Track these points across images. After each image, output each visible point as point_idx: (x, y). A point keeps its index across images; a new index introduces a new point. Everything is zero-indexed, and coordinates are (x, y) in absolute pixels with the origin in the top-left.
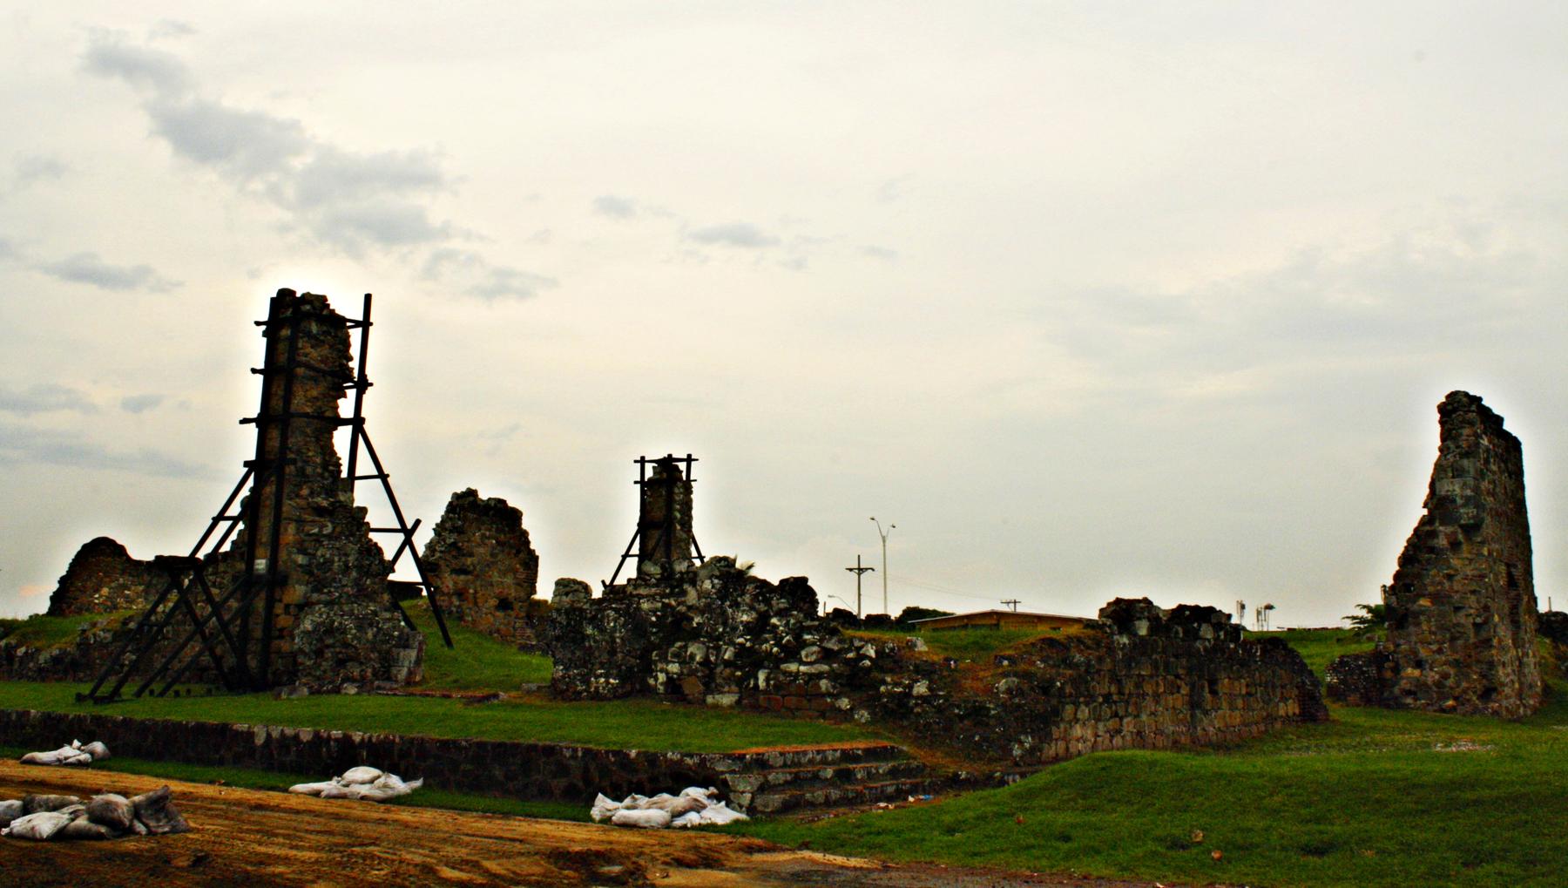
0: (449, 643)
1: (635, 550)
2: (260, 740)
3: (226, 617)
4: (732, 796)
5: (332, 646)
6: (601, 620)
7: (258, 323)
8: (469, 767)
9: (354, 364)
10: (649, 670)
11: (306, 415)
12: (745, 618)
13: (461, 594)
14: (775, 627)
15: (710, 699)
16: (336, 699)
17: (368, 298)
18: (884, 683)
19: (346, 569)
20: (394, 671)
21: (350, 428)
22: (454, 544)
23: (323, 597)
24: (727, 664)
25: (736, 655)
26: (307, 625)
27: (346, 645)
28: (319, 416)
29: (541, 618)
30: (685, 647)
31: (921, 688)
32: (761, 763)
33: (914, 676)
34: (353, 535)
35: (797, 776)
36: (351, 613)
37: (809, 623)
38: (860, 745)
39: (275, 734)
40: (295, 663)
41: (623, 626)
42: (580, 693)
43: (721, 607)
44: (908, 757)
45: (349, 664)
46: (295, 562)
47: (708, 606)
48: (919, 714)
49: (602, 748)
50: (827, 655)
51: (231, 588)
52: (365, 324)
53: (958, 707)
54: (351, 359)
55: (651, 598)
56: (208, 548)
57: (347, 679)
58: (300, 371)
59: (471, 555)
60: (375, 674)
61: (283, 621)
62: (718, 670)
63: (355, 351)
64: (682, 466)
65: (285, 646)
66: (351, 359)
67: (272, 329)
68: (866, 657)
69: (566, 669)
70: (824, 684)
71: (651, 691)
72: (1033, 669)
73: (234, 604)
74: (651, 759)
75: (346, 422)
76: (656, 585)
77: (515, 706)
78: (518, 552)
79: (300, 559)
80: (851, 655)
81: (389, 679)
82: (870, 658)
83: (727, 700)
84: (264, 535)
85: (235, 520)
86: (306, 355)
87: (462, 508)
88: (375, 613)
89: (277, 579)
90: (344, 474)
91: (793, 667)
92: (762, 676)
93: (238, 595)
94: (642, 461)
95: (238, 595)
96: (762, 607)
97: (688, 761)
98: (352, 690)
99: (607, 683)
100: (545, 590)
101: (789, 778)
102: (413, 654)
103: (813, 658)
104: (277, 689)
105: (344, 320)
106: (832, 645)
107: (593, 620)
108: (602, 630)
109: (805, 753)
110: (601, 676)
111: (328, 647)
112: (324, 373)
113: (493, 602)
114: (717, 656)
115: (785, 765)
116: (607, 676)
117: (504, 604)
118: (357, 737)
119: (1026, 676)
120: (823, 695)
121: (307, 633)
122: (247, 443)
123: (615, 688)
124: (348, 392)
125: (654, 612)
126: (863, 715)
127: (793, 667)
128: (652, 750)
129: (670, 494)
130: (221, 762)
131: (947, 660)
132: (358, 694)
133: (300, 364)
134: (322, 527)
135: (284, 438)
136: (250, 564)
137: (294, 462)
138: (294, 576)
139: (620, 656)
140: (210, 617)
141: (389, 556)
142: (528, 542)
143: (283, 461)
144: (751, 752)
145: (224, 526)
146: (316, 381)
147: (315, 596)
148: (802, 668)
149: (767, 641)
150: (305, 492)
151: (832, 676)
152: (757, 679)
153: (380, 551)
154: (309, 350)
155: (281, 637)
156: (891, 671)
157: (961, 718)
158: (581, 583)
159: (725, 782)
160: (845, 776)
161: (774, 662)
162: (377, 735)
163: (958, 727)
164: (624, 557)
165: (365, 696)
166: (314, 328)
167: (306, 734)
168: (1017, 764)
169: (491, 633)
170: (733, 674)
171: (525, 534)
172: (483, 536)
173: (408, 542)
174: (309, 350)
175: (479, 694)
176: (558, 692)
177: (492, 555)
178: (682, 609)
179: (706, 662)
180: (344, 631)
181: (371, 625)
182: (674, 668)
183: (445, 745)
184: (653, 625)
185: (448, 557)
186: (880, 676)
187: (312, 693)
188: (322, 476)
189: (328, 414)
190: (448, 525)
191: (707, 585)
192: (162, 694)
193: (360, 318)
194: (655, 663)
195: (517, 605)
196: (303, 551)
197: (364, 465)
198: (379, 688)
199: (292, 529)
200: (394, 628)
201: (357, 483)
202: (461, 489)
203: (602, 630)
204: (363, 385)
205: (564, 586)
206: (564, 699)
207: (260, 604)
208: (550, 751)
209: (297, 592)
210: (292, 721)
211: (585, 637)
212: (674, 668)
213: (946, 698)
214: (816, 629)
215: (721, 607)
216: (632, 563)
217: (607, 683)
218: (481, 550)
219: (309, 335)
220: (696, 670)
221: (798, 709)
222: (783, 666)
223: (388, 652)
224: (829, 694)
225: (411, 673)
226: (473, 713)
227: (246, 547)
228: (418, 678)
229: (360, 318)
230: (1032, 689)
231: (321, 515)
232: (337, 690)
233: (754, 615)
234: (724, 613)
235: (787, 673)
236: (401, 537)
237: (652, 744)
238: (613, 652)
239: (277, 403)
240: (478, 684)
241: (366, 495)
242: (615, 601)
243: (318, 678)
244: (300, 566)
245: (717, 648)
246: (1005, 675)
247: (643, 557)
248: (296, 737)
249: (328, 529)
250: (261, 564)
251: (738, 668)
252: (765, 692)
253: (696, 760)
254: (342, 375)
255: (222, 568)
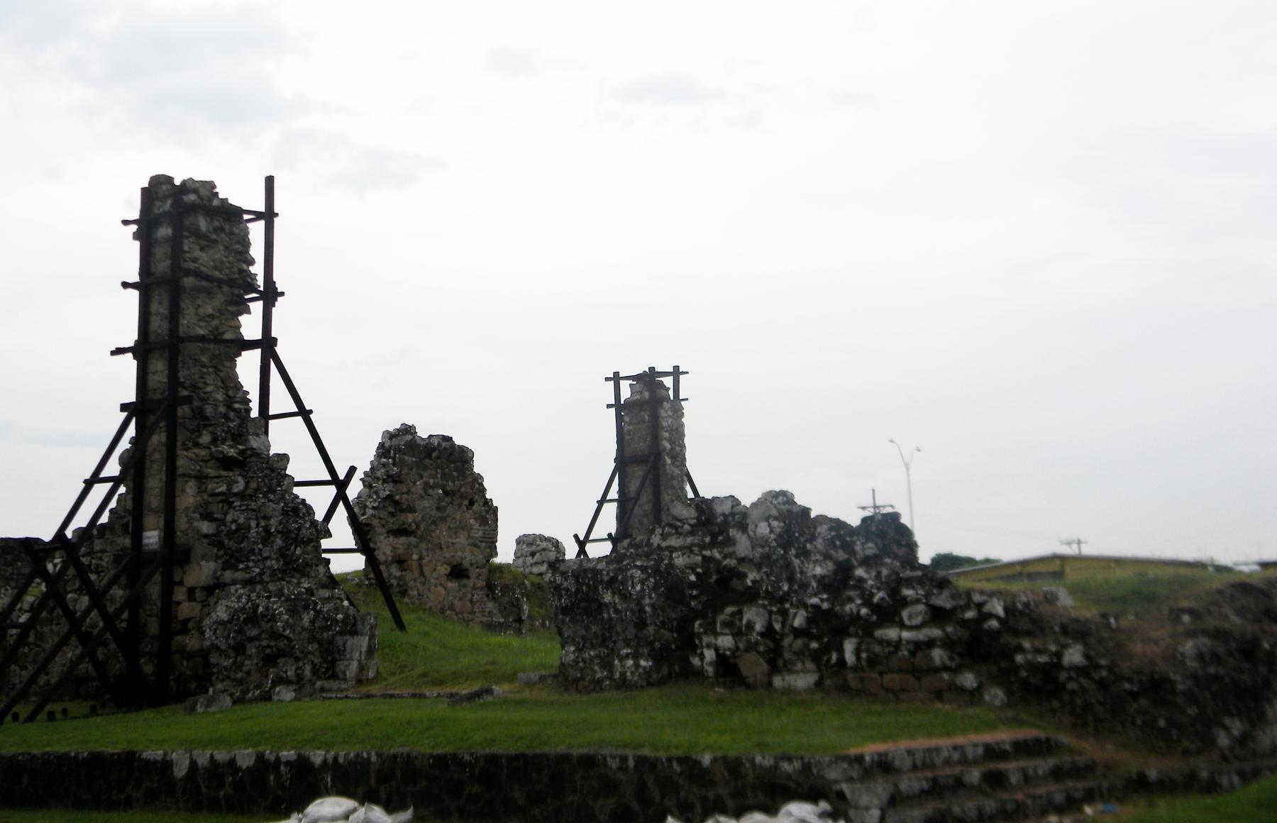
0: (400, 624)
1: (613, 494)
2: (180, 771)
3: (111, 609)
4: (852, 813)
5: (258, 638)
6: (623, 583)
7: (609, 406)
8: (476, 788)
9: (258, 269)
10: (690, 644)
11: (202, 339)
12: (818, 571)
13: (401, 562)
14: (861, 580)
15: (778, 681)
16: (264, 707)
17: (270, 181)
18: (1021, 649)
19: (267, 536)
20: (340, 666)
21: (257, 353)
22: (389, 497)
23: (239, 575)
24: (798, 633)
25: (809, 621)
26: (221, 613)
27: (276, 636)
28: (217, 339)
29: (506, 588)
30: (740, 613)
31: (1074, 655)
32: (884, 766)
33: (1063, 640)
34: (274, 492)
35: (935, 781)
36: (280, 594)
37: (908, 573)
38: (1004, 736)
39: (202, 761)
40: (207, 664)
41: (655, 588)
42: (600, 682)
43: (785, 557)
44: (1070, 751)
45: (282, 661)
46: (198, 532)
47: (767, 558)
48: (1073, 692)
49: (662, 755)
50: (937, 615)
51: (113, 572)
52: (269, 216)
53: (1130, 680)
54: (252, 262)
55: (688, 550)
56: (81, 520)
57: (281, 681)
58: (188, 281)
59: (412, 510)
60: (315, 672)
61: (186, 610)
62: (786, 642)
63: (257, 250)
64: (668, 382)
65: (192, 642)
66: (252, 262)
67: (146, 228)
68: (991, 616)
69: (579, 650)
70: (938, 655)
71: (698, 674)
72: (1227, 625)
73: (118, 592)
74: (733, 767)
75: (251, 345)
76: (692, 533)
77: (520, 703)
78: (472, 503)
79: (206, 527)
80: (970, 614)
81: (334, 677)
82: (998, 618)
83: (802, 680)
84: (154, 499)
85: (116, 481)
86: (195, 260)
87: (398, 450)
88: (310, 592)
89: (175, 555)
90: (255, 413)
91: (892, 633)
92: (849, 647)
93: (123, 580)
94: (616, 378)
95: (123, 580)
96: (841, 555)
97: (786, 767)
98: (287, 694)
99: (637, 665)
100: (505, 553)
101: (925, 785)
102: (363, 642)
103: (918, 620)
104: (190, 700)
105: (239, 212)
106: (943, 601)
107: (611, 583)
108: (626, 597)
109: (938, 750)
110: (627, 655)
111: (251, 639)
112: (220, 283)
113: (444, 570)
114: (783, 624)
115: (915, 767)
116: (636, 656)
117: (458, 572)
118: (317, 757)
119: (1220, 635)
120: (937, 670)
121: (223, 623)
122: (123, 380)
123: (647, 673)
124: (251, 305)
125: (693, 568)
126: (996, 695)
127: (892, 633)
128: (732, 753)
129: (655, 418)
130: (128, 804)
131: (1105, 616)
132: (296, 699)
133: (187, 273)
134: (230, 484)
135: (173, 370)
136: (137, 537)
137: (188, 400)
138: (199, 549)
139: (651, 629)
140: (87, 612)
141: (319, 516)
142: (483, 490)
143: (173, 401)
144: (870, 750)
145: (100, 491)
146: (210, 294)
147: (228, 575)
148: (906, 635)
149: (851, 600)
150: (205, 438)
151: (948, 643)
152: (841, 651)
153: (309, 510)
154: (197, 253)
155: (185, 631)
156: (1029, 634)
157: (1134, 696)
158: (549, 539)
159: (841, 795)
160: (995, 780)
161: (866, 629)
162: (345, 753)
163: (1133, 707)
164: (601, 503)
165: (306, 702)
166: (203, 224)
167: (245, 758)
168: (1225, 759)
169: (443, 611)
170: (807, 646)
171: (478, 479)
172: (426, 484)
173: (341, 496)
174: (196, 260)
175: (465, 690)
176: (567, 680)
177: (439, 509)
178: (730, 562)
179: (769, 632)
180: (273, 619)
181: (306, 607)
182: (726, 642)
183: (440, 760)
184: (692, 585)
185: (383, 514)
186: (1013, 641)
187: (235, 702)
188: (226, 416)
189: (229, 336)
190: (381, 473)
191: (763, 529)
192: (31, 718)
193: (261, 208)
194: (699, 636)
195: (473, 572)
196: (207, 516)
197: (280, 400)
198: (323, 690)
199: (191, 487)
200: (337, 610)
201: (271, 422)
202: (393, 426)
203: (626, 597)
204: (270, 295)
205: (528, 544)
206: (578, 691)
207: (154, 589)
208: (589, 761)
209: (202, 571)
210: (222, 742)
211: (601, 607)
212: (726, 642)
213: (1111, 669)
214: (920, 581)
215: (785, 557)
216: (610, 510)
217: (637, 665)
218: (426, 503)
219: (196, 233)
220: (757, 643)
221: (903, 690)
222: (879, 633)
223: (332, 642)
224: (946, 668)
225: (361, 668)
226: (468, 715)
227: (130, 517)
228: (371, 675)
229: (261, 208)
230: (1229, 653)
231: (227, 468)
232: (267, 697)
233: (831, 566)
234: (788, 565)
235: (884, 642)
236: (332, 490)
237: (733, 746)
238: (641, 624)
239: (156, 324)
240: (456, 677)
241: (285, 438)
242: (639, 556)
243: (240, 682)
244: (206, 536)
245: (784, 613)
246: (1190, 634)
247: (625, 505)
248: (232, 762)
249: (240, 486)
250: (152, 538)
251: (813, 638)
252: (856, 669)
253: (797, 765)
254: (240, 284)
255: (98, 545)
